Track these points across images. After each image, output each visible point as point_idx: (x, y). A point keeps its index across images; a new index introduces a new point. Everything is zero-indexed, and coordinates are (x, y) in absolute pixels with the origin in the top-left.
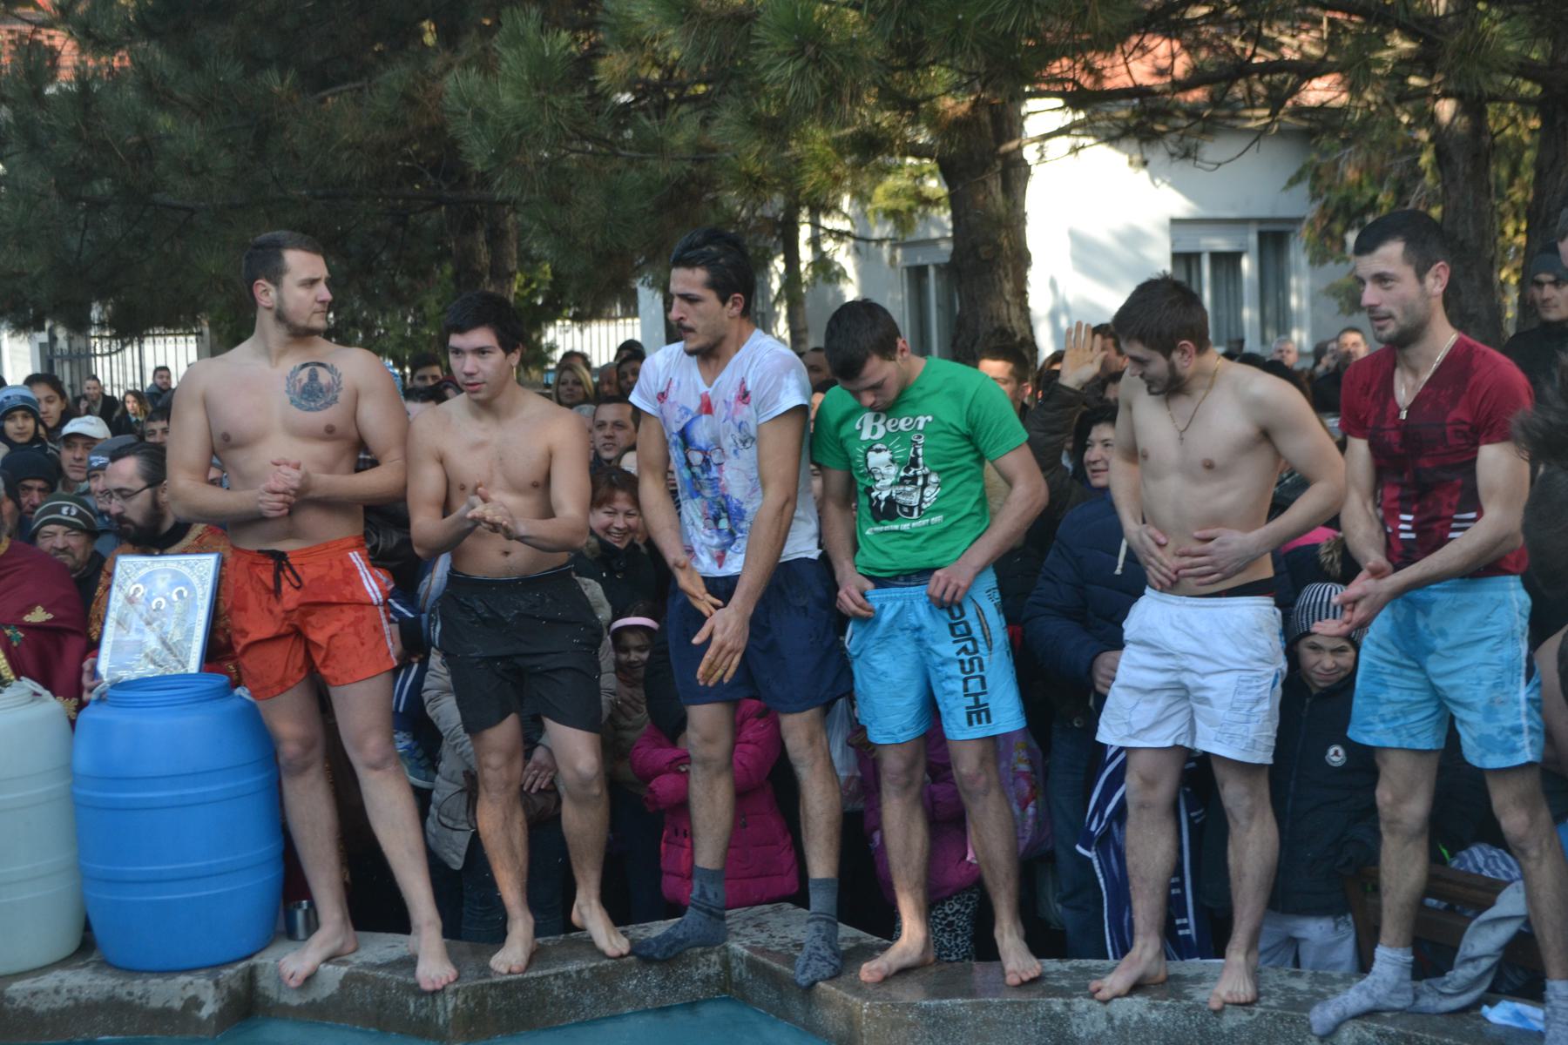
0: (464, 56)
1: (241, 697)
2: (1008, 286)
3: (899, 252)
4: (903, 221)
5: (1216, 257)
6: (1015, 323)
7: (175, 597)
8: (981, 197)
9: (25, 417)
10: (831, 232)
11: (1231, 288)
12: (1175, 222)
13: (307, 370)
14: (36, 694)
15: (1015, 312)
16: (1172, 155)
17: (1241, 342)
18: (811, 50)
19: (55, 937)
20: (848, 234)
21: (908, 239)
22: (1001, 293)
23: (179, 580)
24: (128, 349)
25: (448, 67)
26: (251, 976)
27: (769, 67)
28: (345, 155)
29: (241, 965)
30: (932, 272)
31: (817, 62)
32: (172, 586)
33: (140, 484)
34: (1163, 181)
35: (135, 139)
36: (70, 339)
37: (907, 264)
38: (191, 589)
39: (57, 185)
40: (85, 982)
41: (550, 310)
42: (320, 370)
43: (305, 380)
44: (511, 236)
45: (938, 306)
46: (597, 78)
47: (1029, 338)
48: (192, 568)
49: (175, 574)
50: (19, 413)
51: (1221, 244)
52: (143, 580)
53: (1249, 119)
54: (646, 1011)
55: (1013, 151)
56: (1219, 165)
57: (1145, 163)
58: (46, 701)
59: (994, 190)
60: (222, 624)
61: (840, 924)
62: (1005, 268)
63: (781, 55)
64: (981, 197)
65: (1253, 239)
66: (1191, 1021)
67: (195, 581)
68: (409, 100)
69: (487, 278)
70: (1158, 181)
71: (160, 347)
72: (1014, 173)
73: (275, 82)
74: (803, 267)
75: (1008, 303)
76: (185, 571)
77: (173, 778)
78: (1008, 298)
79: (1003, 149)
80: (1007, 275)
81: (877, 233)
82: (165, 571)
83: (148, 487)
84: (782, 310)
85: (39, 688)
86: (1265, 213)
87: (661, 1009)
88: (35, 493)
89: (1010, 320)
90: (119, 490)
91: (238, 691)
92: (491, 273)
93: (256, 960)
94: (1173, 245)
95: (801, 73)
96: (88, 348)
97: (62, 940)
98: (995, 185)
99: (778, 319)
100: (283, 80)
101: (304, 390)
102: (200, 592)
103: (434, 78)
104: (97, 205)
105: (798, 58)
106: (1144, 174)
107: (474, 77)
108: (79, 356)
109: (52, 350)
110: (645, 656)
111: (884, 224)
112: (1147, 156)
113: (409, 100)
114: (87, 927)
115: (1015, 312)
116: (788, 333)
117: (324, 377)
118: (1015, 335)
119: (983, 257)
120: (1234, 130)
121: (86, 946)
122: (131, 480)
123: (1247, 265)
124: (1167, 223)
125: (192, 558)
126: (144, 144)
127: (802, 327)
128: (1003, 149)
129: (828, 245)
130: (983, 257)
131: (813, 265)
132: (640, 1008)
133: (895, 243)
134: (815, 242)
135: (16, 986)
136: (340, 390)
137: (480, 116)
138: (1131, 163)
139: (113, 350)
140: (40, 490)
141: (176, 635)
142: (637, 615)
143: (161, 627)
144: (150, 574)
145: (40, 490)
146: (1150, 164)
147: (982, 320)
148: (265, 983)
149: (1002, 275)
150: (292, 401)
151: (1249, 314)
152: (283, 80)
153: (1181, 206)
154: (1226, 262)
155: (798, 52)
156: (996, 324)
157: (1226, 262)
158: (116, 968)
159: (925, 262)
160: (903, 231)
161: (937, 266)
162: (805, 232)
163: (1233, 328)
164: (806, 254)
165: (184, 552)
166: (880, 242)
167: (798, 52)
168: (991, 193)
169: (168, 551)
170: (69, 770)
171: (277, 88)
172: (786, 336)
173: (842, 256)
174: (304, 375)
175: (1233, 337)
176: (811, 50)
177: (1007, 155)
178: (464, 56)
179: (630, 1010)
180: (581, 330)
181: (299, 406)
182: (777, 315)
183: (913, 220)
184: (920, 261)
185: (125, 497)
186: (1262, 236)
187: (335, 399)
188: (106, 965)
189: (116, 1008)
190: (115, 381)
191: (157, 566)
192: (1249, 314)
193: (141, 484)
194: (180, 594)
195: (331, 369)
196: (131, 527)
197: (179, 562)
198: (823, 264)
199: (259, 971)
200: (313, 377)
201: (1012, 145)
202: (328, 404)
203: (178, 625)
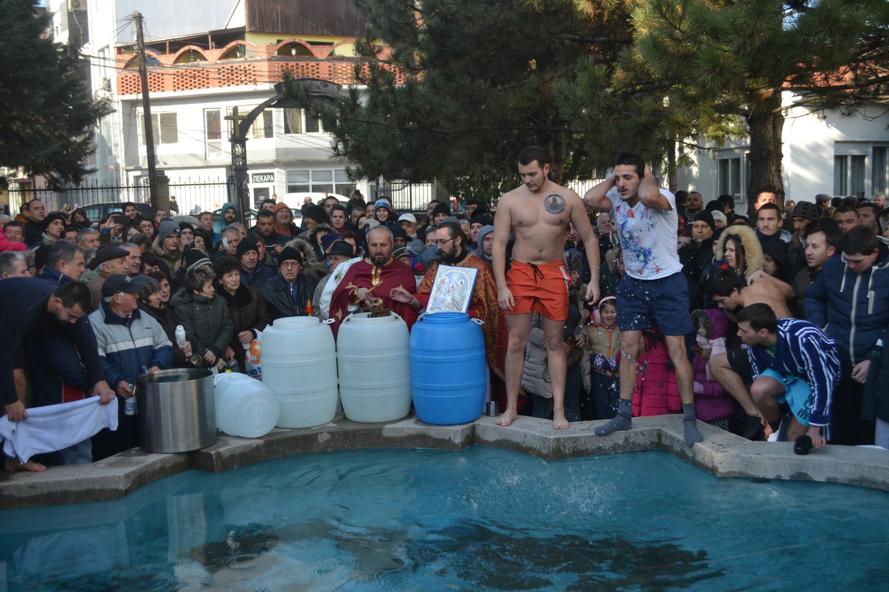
0: (559, 74)
1: (473, 322)
2: (773, 168)
3: (716, 153)
4: (720, 141)
5: (854, 157)
6: (775, 183)
7: (459, 283)
8: (763, 131)
9: (384, 211)
10: (688, 145)
11: (860, 171)
12: (837, 142)
13: (552, 198)
14: (396, 318)
15: (776, 179)
16: (843, 114)
17: (863, 193)
18: (718, 69)
19: (397, 408)
20: (696, 146)
21: (721, 148)
22: (770, 171)
23: (462, 277)
24: (406, 188)
25: (552, 79)
26: (473, 429)
27: (700, 75)
28: (510, 112)
29: (470, 424)
30: (730, 161)
31: (720, 74)
32: (459, 279)
33: (449, 238)
34: (832, 125)
35: (429, 107)
36: (384, 184)
37: (720, 158)
38: (466, 281)
39: (398, 124)
40: (410, 427)
41: (571, 175)
42: (556, 197)
43: (551, 202)
44: (563, 145)
45: (732, 176)
46: (612, 82)
47: (781, 190)
48: (467, 273)
49: (461, 274)
50: (382, 209)
51: (856, 152)
52: (448, 275)
53: (881, 99)
54: (627, 452)
55: (778, 112)
56: (874, 118)
57: (825, 118)
58: (400, 320)
59: (769, 128)
60: (476, 294)
61: (697, 420)
62: (772, 160)
63: (705, 71)
64: (763, 131)
65: (870, 150)
66: (856, 470)
67: (468, 278)
68: (538, 91)
69: (553, 162)
70: (830, 125)
71: (418, 188)
72: (778, 121)
73: (481, 83)
74: (676, 159)
75: (773, 175)
76: (464, 274)
77: (447, 352)
78: (773, 173)
79: (774, 111)
80: (773, 164)
81: (707, 145)
82: (456, 273)
83: (452, 239)
84: (666, 177)
85: (397, 316)
86: (876, 139)
87: (633, 452)
88: (399, 242)
89: (773, 182)
90: (441, 240)
91: (473, 319)
92: (555, 160)
93: (476, 423)
94: (835, 152)
95: (713, 79)
96: (391, 188)
97: (403, 410)
98: (770, 127)
99: (664, 180)
100: (485, 84)
101: (551, 205)
102: (469, 283)
103: (547, 82)
104: (410, 131)
105: (712, 73)
106: (824, 122)
107: (564, 82)
108: (387, 191)
109: (377, 188)
110: (614, 315)
111: (711, 142)
112: (826, 114)
113: (538, 91)
114: (412, 406)
115: (776, 179)
116: (668, 186)
117: (559, 201)
118: (776, 188)
119: (764, 156)
120: (875, 105)
121: (412, 412)
122: (445, 236)
123: (867, 161)
124: (833, 143)
125: (467, 269)
126: (432, 109)
127: (675, 183)
128: (774, 111)
129: (687, 150)
130: (764, 156)
131: (680, 158)
132: (624, 451)
133: (715, 150)
134: (681, 149)
135: (387, 426)
136: (565, 206)
137: (567, 98)
138: (818, 118)
139: (400, 188)
140: (401, 240)
141: (458, 298)
142: (608, 296)
143: (453, 295)
144: (451, 273)
145: (401, 240)
146: (827, 118)
147: (761, 181)
148: (479, 432)
149: (771, 163)
150: (547, 210)
151: (868, 182)
152: (485, 84)
153: (835, 134)
154: (858, 160)
155: (713, 70)
156: (768, 184)
157: (858, 160)
158: (424, 422)
159: (727, 158)
160: (719, 145)
161: (731, 159)
162: (677, 145)
163: (860, 187)
164: (677, 154)
165: (464, 266)
166: (709, 149)
167: (713, 70)
168: (768, 129)
169: (458, 264)
170: (408, 347)
171: (483, 87)
172: (668, 187)
173: (693, 156)
174: (551, 199)
175: (860, 191)
176: (718, 69)
177: (775, 114)
178: (559, 74)
179: (620, 451)
180: (582, 184)
181: (550, 212)
182: (663, 179)
183: (724, 140)
184: (725, 157)
185: (443, 243)
186: (875, 149)
187: (563, 209)
188: (419, 421)
189: (423, 438)
190: (401, 201)
191: (454, 270)
192: (868, 182)
193: (450, 238)
194: (461, 282)
195: (561, 198)
196: (445, 255)
197: (462, 270)
198: (684, 158)
199: (476, 427)
200: (555, 201)
201: (778, 109)
202: (561, 211)
203: (459, 294)
